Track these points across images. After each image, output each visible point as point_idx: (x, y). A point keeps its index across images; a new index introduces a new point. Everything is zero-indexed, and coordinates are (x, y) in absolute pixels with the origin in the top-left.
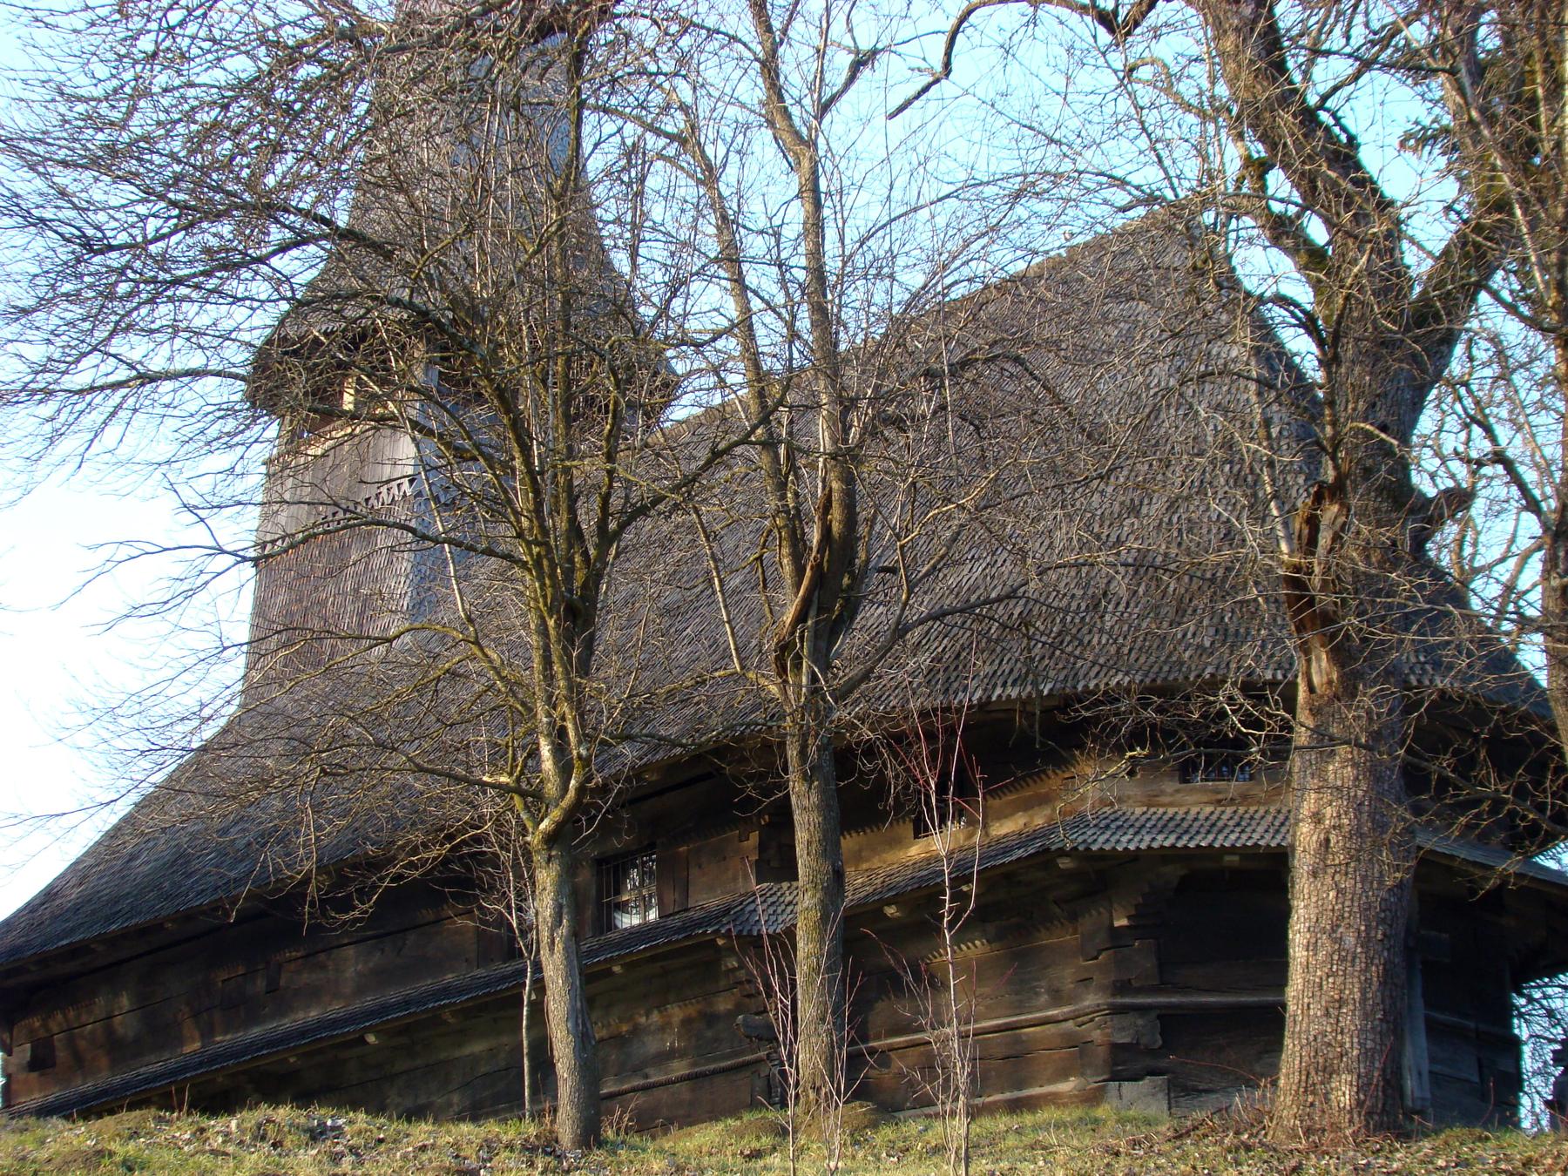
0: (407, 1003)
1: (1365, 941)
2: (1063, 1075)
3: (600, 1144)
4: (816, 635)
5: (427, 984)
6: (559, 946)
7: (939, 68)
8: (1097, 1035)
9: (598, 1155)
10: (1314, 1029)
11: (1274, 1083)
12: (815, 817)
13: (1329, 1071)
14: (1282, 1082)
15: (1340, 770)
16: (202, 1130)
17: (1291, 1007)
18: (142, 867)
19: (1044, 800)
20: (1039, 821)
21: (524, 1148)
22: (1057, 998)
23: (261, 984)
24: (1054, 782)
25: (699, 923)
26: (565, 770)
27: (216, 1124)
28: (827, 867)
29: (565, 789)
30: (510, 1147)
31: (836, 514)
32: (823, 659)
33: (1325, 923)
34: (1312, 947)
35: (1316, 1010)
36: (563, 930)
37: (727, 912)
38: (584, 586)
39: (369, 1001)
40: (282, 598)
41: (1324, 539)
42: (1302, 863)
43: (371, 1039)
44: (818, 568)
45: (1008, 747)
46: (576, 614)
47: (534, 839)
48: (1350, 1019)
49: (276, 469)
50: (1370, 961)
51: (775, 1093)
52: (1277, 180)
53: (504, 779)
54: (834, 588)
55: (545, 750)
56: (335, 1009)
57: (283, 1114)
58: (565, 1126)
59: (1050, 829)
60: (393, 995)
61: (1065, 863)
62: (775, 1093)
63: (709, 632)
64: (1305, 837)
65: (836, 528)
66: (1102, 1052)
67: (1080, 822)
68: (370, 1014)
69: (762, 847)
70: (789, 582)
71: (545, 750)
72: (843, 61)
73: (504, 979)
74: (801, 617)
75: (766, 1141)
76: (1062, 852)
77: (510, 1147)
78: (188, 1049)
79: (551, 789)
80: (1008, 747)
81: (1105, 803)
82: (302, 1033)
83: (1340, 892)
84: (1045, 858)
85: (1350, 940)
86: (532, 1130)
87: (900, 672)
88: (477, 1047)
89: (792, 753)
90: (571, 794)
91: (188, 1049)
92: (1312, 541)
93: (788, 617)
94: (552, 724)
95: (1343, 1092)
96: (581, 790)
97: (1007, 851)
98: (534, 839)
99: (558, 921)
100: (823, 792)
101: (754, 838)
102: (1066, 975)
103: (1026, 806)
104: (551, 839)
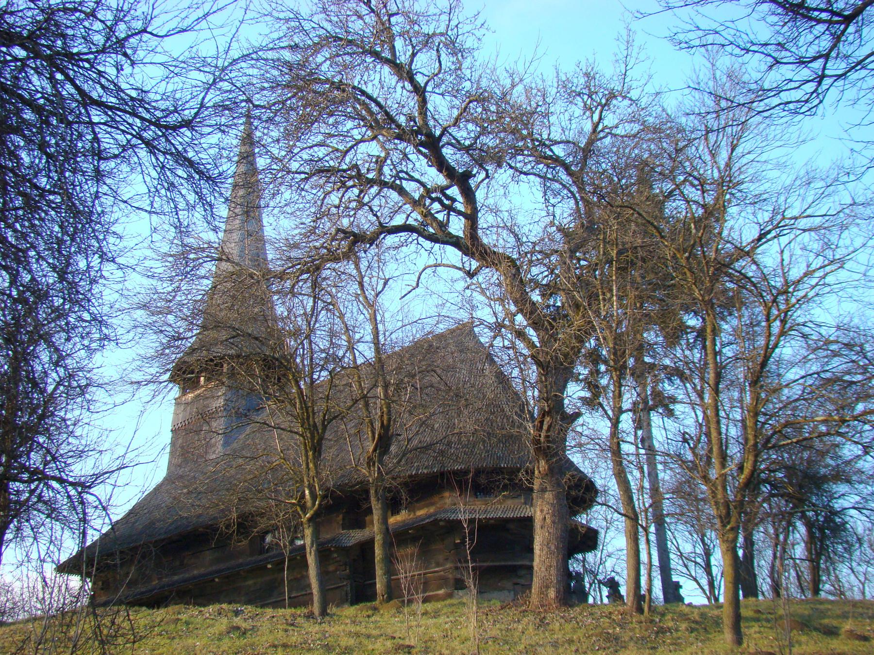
0: (228, 569)
1: (557, 548)
2: (439, 588)
3: (328, 614)
4: (380, 453)
5: (233, 563)
6: (313, 553)
7: (414, 285)
8: (450, 576)
9: (327, 618)
10: (543, 575)
11: (531, 592)
12: (380, 512)
13: (547, 587)
14: (533, 591)
15: (549, 496)
16: (201, 611)
17: (535, 568)
18: (139, 526)
19: (432, 504)
20: (432, 510)
21: (304, 616)
22: (438, 565)
23: (178, 563)
24: (436, 499)
25: (325, 543)
26: (314, 496)
27: (204, 609)
28: (384, 527)
29: (314, 504)
30: (300, 616)
31: (385, 417)
32: (381, 461)
33: (545, 543)
34: (541, 550)
35: (543, 569)
36: (314, 548)
37: (334, 539)
38: (318, 441)
39: (214, 568)
40: (180, 441)
41: (545, 427)
42: (537, 524)
43: (217, 580)
44: (380, 435)
45: (425, 488)
46: (317, 449)
47: (304, 520)
48: (553, 571)
49: (178, 402)
50: (558, 554)
51: (372, 597)
52: (519, 318)
53: (294, 501)
54: (384, 443)
55: (307, 492)
56: (202, 571)
57: (224, 606)
58: (316, 608)
59: (435, 514)
60: (222, 566)
61: (441, 523)
62: (372, 597)
63: (352, 455)
64: (538, 517)
65: (385, 422)
66: (452, 582)
67: (446, 511)
68: (217, 572)
69: (343, 519)
70: (370, 439)
71: (307, 492)
72: (382, 282)
73: (261, 561)
74: (375, 450)
75: (370, 612)
76: (441, 520)
77: (300, 616)
78: (154, 583)
79: (309, 504)
80: (425, 488)
81: (463, 508)
82: (194, 578)
83: (549, 533)
84: (435, 522)
85: (553, 547)
86: (306, 611)
87: (400, 466)
88: (250, 582)
89: (372, 492)
90: (316, 506)
91: (154, 583)
92: (541, 427)
93: (371, 450)
94: (309, 484)
95: (552, 593)
96: (320, 505)
97: (423, 520)
98: (304, 520)
99: (312, 546)
100: (382, 503)
101: (341, 516)
102: (441, 558)
103: (427, 506)
104: (310, 520)
